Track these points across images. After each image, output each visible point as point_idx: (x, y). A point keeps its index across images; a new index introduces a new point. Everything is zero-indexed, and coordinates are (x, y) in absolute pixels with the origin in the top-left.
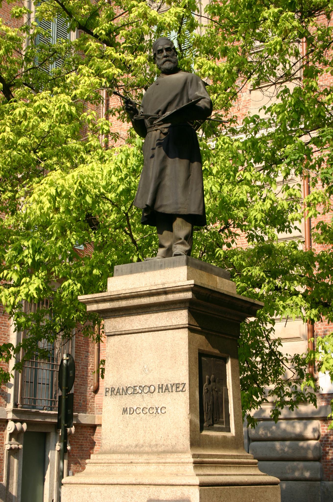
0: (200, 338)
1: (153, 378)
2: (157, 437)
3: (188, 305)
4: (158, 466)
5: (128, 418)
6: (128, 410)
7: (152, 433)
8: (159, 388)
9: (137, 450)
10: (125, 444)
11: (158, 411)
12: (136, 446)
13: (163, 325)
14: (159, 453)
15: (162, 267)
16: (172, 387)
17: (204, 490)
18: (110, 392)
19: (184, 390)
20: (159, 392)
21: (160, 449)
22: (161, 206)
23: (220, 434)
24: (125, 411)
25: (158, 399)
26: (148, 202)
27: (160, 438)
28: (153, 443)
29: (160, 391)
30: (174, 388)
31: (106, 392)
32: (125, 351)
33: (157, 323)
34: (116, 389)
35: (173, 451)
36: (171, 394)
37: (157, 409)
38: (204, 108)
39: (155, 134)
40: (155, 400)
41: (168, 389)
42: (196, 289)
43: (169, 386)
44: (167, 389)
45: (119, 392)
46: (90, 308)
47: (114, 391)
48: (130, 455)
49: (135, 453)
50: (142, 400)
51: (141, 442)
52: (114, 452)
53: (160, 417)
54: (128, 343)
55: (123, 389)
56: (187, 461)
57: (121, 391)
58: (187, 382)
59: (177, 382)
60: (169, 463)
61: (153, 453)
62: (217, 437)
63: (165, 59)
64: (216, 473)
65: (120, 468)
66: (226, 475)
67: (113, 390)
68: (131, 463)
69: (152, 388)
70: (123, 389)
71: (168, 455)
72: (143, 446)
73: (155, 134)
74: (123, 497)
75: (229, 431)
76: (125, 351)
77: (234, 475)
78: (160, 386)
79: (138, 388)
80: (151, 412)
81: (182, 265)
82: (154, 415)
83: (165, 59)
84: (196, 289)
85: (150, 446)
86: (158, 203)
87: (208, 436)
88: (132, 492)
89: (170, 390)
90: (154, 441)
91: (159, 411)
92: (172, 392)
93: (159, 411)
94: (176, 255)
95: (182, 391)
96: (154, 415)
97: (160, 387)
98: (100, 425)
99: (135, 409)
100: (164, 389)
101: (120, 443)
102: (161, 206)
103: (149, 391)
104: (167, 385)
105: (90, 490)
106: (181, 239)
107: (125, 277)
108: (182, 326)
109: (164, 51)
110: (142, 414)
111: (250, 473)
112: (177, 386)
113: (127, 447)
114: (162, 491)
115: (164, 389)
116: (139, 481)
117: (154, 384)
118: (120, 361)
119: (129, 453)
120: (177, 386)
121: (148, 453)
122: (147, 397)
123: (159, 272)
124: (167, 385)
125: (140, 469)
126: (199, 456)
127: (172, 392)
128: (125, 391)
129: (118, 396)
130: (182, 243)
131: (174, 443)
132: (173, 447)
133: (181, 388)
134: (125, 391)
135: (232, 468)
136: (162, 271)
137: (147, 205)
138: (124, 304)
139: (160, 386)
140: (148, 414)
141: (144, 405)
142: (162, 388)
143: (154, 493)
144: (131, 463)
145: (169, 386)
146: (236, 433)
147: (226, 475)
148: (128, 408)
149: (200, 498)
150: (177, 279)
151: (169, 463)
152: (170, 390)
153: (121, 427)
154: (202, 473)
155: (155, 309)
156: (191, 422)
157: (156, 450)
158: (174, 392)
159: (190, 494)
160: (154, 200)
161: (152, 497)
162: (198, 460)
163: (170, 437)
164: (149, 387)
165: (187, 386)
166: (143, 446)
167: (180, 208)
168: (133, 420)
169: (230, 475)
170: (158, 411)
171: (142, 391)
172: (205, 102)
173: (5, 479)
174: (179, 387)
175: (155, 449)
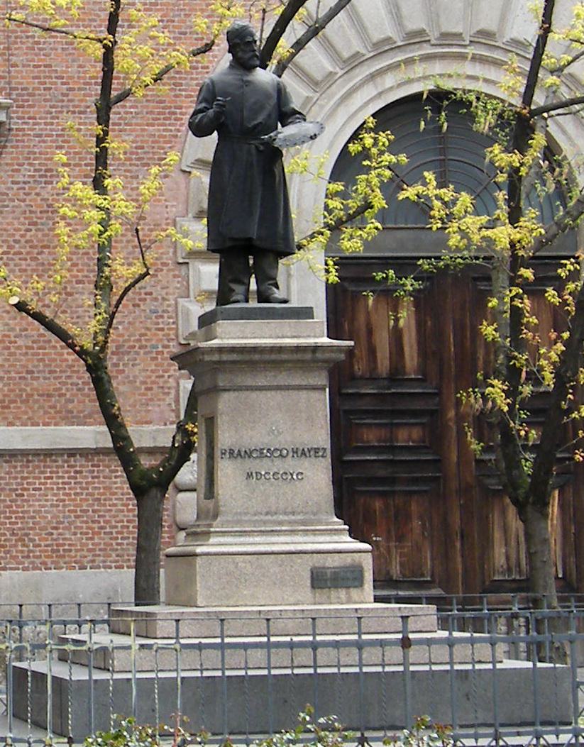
1: (286, 440)
6: (254, 475)
11: (287, 477)
16: (309, 452)
24: (249, 475)
25: (291, 464)
30: (312, 453)
31: (222, 454)
34: (236, 452)
37: (292, 475)
43: (306, 450)
45: (241, 455)
46: (207, 358)
47: (232, 454)
50: (270, 464)
51: (273, 509)
57: (243, 453)
58: (328, 446)
67: (231, 452)
79: (265, 451)
91: (295, 477)
93: (295, 477)
97: (295, 451)
99: (263, 473)
100: (304, 453)
103: (281, 455)
104: (303, 450)
105: (236, 561)
112: (316, 450)
122: (278, 462)
124: (303, 450)
128: (249, 454)
133: (320, 454)
134: (249, 454)
138: (256, 357)
141: (276, 470)
142: (297, 452)
143: (318, 561)
152: (308, 455)
155: (289, 365)
161: (316, 565)
164: (281, 451)
171: (272, 454)
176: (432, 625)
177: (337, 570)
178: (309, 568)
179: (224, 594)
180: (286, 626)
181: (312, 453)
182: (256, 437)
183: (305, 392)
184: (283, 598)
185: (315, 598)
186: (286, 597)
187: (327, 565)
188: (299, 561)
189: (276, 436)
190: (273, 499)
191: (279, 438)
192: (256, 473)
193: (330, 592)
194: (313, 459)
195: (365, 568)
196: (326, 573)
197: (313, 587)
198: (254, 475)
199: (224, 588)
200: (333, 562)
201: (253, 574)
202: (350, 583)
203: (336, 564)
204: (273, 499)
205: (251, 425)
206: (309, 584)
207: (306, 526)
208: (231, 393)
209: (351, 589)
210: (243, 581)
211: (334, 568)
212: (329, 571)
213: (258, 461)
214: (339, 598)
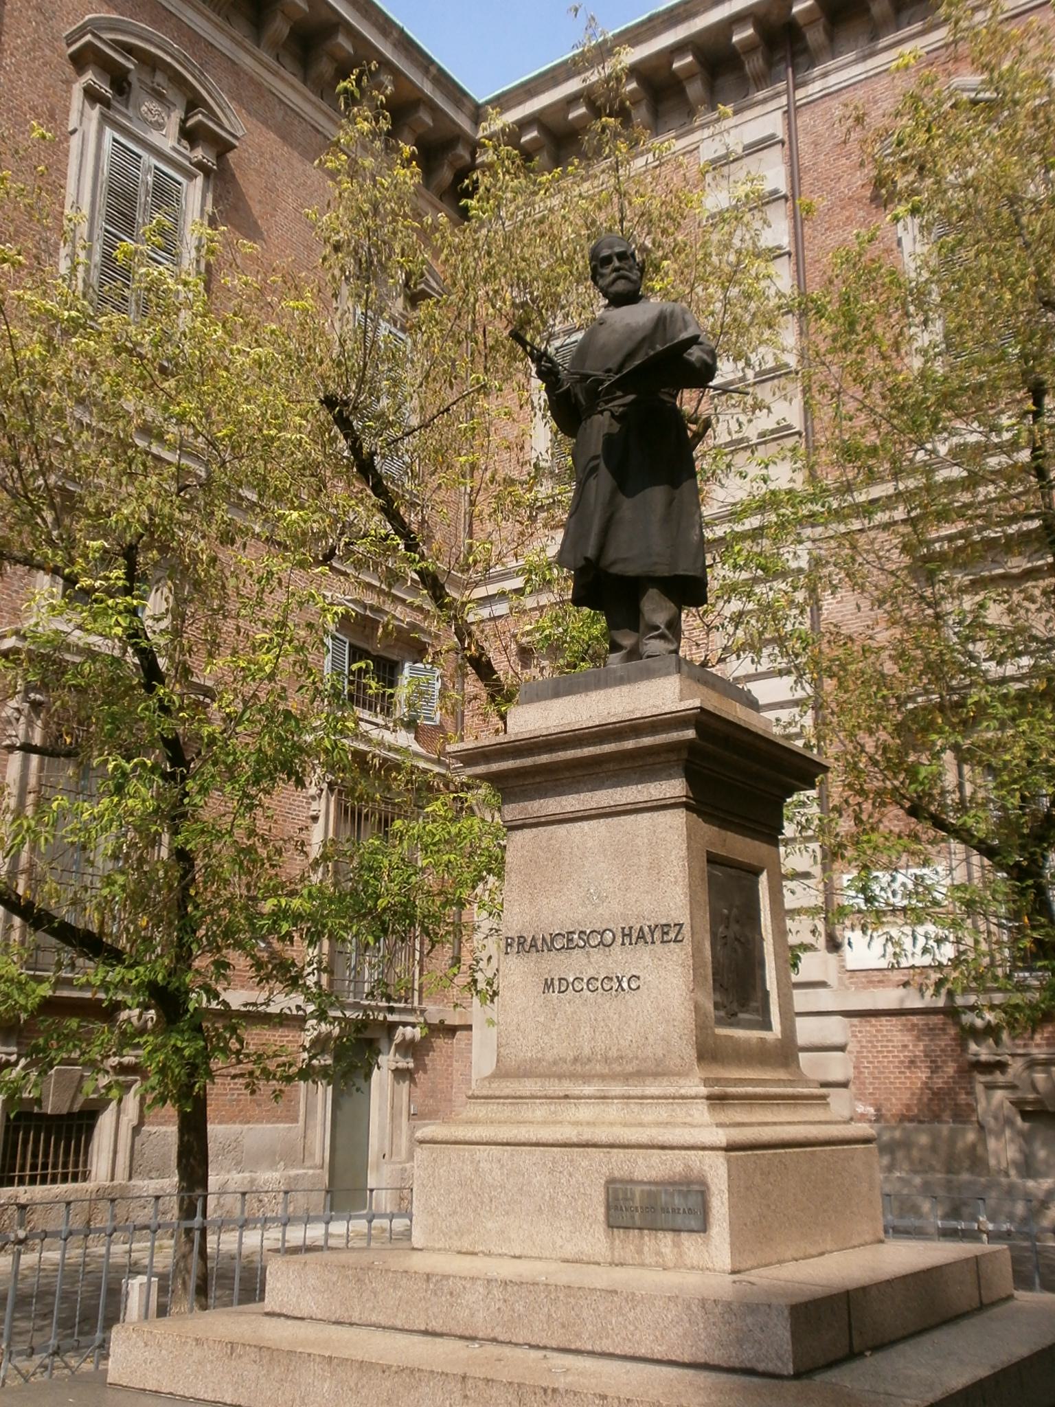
0: (709, 831)
1: (611, 912)
2: (622, 1042)
3: (685, 755)
4: (627, 1104)
5: (556, 1001)
6: (556, 983)
7: (610, 1031)
8: (624, 935)
9: (578, 1069)
10: (549, 1056)
11: (614, 985)
12: (576, 1060)
13: (629, 801)
14: (627, 1077)
15: (621, 681)
17: (737, 1158)
18: (515, 945)
19: (680, 938)
20: (623, 944)
21: (629, 1068)
22: (613, 563)
23: (755, 1034)
24: (548, 985)
25: (621, 961)
26: (591, 552)
27: (627, 1043)
28: (613, 1053)
29: (627, 941)
30: (657, 935)
31: (508, 945)
32: (547, 859)
33: (617, 797)
34: (529, 940)
35: (658, 1072)
36: (651, 947)
37: (620, 982)
38: (698, 365)
39: (601, 424)
40: (616, 962)
41: (643, 937)
42: (704, 718)
43: (646, 929)
44: (641, 936)
45: (535, 946)
48: (563, 1081)
49: (573, 1076)
50: (585, 961)
51: (587, 1051)
52: (527, 1074)
53: (628, 997)
54: (553, 842)
55: (544, 939)
56: (692, 1091)
57: (539, 943)
58: (685, 919)
59: (664, 922)
60: (652, 1098)
61: (614, 1077)
62: (748, 1041)
63: (614, 275)
64: (754, 1119)
65: (540, 1111)
66: (775, 1124)
67: (521, 940)
68: (566, 1097)
69: (609, 935)
70: (544, 939)
71: (649, 1080)
72: (589, 1060)
73: (601, 424)
74: (551, 1171)
75: (768, 1026)
76: (547, 859)
77: (789, 1123)
78: (627, 931)
79: (576, 936)
80: (607, 987)
81: (668, 674)
82: (614, 992)
83: (614, 275)
84: (704, 718)
85: (606, 1060)
86: (612, 554)
87: (731, 1037)
88: (571, 1161)
89: (649, 939)
90: (614, 1049)
91: (625, 985)
92: (653, 942)
93: (625, 985)
94: (649, 657)
95: (676, 941)
96: (614, 992)
98: (469, 1028)
99: (571, 980)
100: (636, 936)
101: (539, 1055)
102: (613, 563)
104: (641, 929)
105: (477, 1157)
106: (657, 628)
107: (543, 704)
108: (673, 801)
109: (615, 259)
110: (586, 993)
111: (806, 1119)
113: (555, 1063)
114: (640, 1161)
115: (636, 936)
116: (588, 1135)
117: (612, 926)
118: (537, 881)
119: (560, 1077)
120: (665, 932)
121: (602, 1077)
122: (597, 955)
123: (617, 689)
124: (641, 929)
125: (585, 1112)
126: (717, 1081)
127: (653, 942)
129: (534, 955)
130: (662, 637)
131: (660, 1053)
132: (659, 1062)
133: (672, 935)
135: (782, 1107)
136: (625, 689)
137: (586, 559)
139: (627, 931)
140: (600, 990)
141: (591, 972)
142: (630, 935)
143: (620, 1164)
144: (566, 1097)
145: (646, 929)
146: (783, 1031)
147: (775, 1124)
148: (556, 978)
149: (729, 1176)
150: (660, 703)
151: (652, 1098)
152: (649, 939)
153: (542, 1019)
154: (727, 1120)
155: (611, 766)
156: (697, 1008)
157: (619, 1069)
158: (658, 943)
159: (706, 1168)
160: (602, 548)
161: (617, 1174)
162: (716, 1090)
163: (651, 1040)
164: (602, 934)
165: (686, 929)
166: (589, 1060)
167: (656, 563)
168: (568, 1003)
169: (781, 1124)
170: (614, 985)
171: (587, 942)
172: (702, 350)
173: (675, 736)
174: (667, 933)
175: (617, 1068)
176: (780, 1358)
177: (653, 1188)
178: (603, 1182)
179: (455, 1227)
180: (472, 1315)
181: (657, 935)
182: (560, 910)
183: (647, 815)
184: (554, 1243)
185: (612, 1249)
186: (559, 1242)
187: (638, 1175)
188: (585, 1163)
189: (596, 906)
190: (585, 1031)
191: (600, 910)
192: (560, 979)
193: (642, 1238)
194: (658, 947)
195: (713, 1189)
196: (633, 1194)
197: (611, 1226)
198: (556, 983)
199: (455, 1212)
200: (650, 1167)
201: (503, 1187)
202: (680, 1220)
203: (653, 1175)
204: (585, 1031)
205: (556, 887)
206: (602, 1218)
207: (634, 1072)
208: (526, 830)
209: (684, 1235)
210: (486, 1200)
211: (649, 1183)
212: (638, 1190)
213: (562, 956)
214: (659, 1253)
